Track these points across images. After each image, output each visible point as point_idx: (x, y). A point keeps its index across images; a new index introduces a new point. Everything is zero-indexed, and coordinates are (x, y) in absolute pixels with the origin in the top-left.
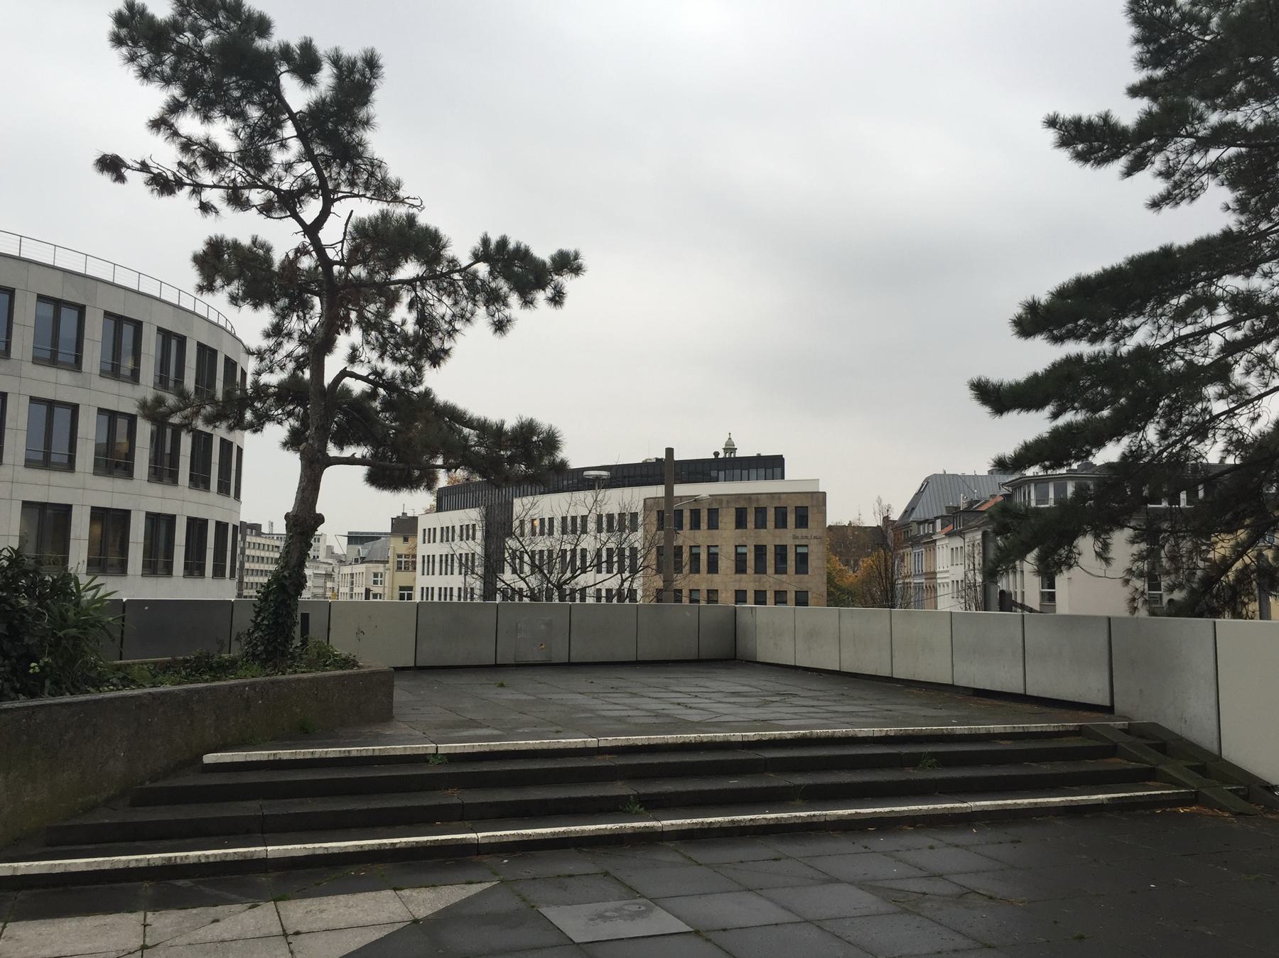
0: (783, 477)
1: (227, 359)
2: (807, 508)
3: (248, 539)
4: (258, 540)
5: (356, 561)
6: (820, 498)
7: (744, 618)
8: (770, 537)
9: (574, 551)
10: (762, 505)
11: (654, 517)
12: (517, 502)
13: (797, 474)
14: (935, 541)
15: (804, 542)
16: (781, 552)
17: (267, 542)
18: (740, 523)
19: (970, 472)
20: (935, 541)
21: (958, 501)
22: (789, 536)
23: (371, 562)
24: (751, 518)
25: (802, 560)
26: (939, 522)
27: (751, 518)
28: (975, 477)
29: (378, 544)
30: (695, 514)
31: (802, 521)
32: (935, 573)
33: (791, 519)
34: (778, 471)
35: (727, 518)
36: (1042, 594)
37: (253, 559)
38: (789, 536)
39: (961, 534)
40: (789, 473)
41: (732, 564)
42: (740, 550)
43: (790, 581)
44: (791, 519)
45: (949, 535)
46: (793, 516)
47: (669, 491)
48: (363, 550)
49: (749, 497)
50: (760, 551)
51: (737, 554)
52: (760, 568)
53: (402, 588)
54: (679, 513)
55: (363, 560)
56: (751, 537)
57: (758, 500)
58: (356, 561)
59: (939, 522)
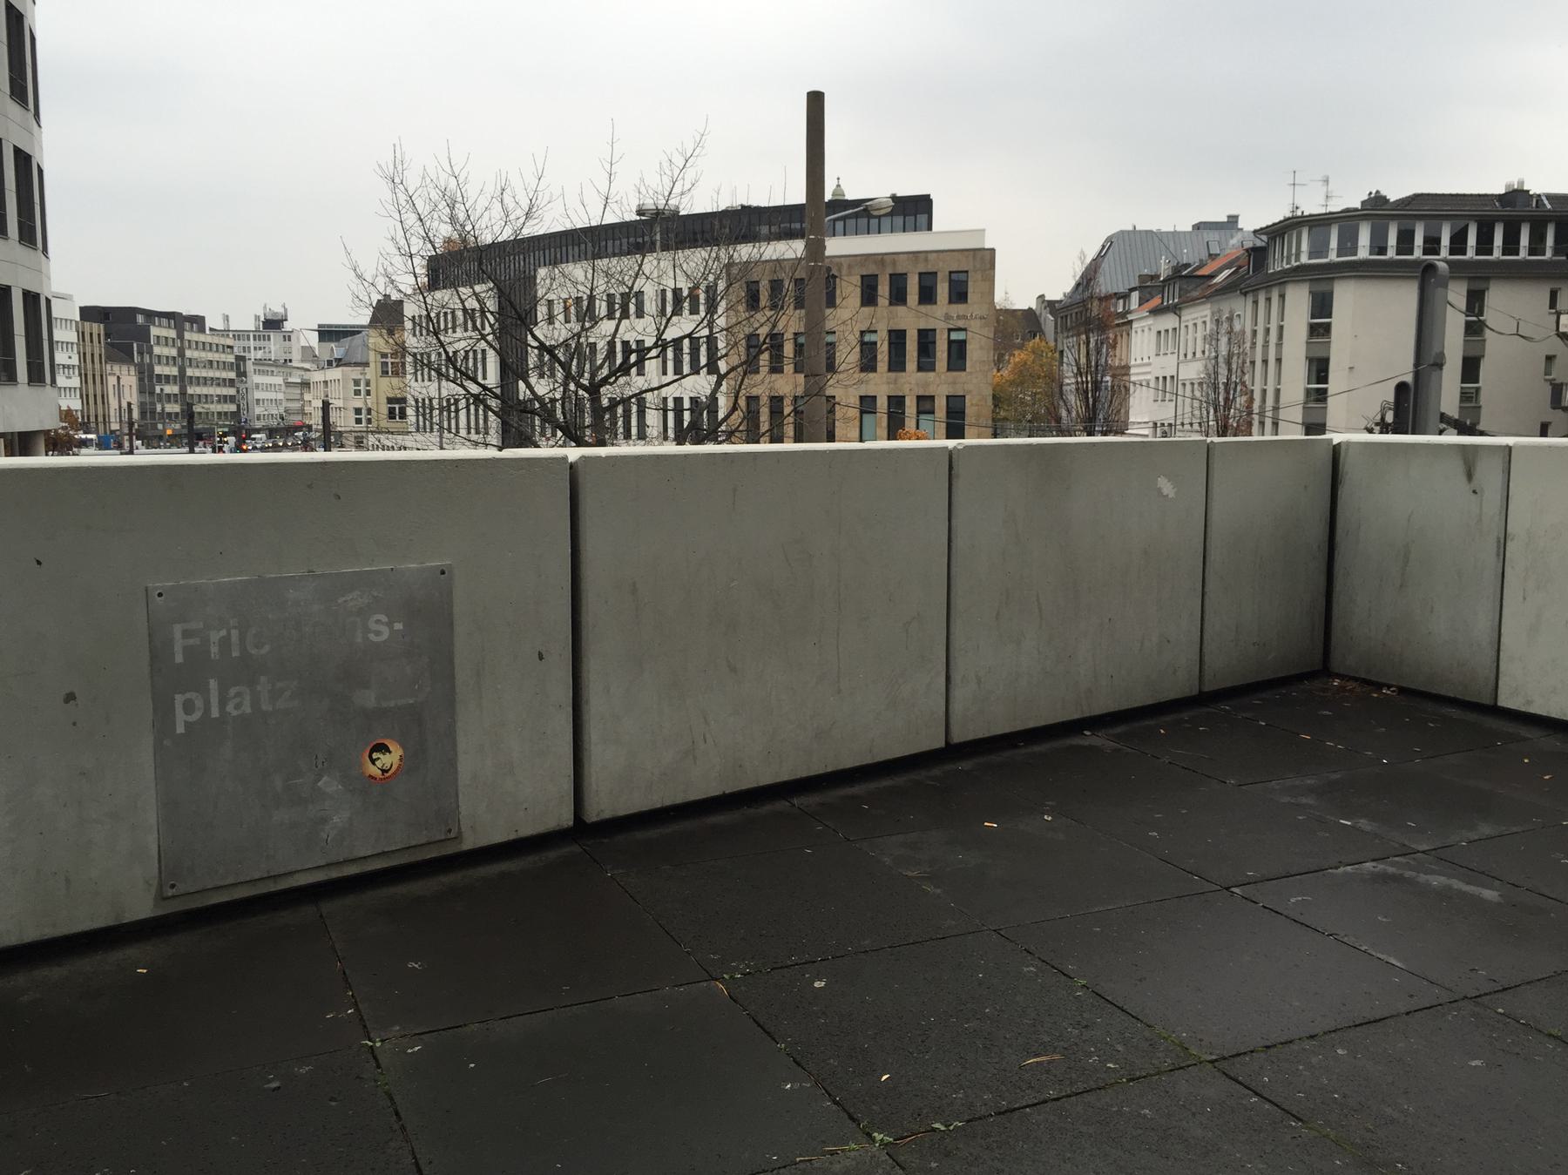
0: (930, 228)
1: (17, 151)
2: (967, 273)
3: (187, 336)
4: (202, 338)
5: (330, 363)
6: (985, 259)
7: (1376, 507)
8: (911, 318)
9: (611, 344)
10: (900, 270)
11: (739, 291)
12: (542, 272)
13: (952, 220)
14: (1131, 322)
15: (961, 324)
16: (926, 340)
17: (216, 340)
18: (869, 296)
19: (1167, 227)
20: (1131, 322)
21: (1158, 265)
22: (939, 316)
23: (348, 364)
24: (884, 289)
25: (958, 353)
26: (1135, 296)
27: (884, 289)
28: (1175, 233)
29: (357, 339)
30: (776, 286)
31: (959, 294)
32: (1127, 367)
33: (943, 290)
34: (922, 218)
35: (849, 291)
36: (1308, 391)
37: (199, 381)
38: (939, 316)
39: (1175, 309)
40: (942, 218)
41: (855, 357)
42: (867, 338)
43: (940, 383)
44: (943, 290)
45: (1156, 312)
46: (946, 285)
47: (815, 249)
48: (336, 349)
49: (880, 259)
50: (897, 338)
51: (863, 344)
52: (897, 364)
53: (390, 401)
54: (831, 280)
55: (339, 362)
56: (885, 317)
57: (894, 263)
58: (330, 363)
59: (1135, 296)
